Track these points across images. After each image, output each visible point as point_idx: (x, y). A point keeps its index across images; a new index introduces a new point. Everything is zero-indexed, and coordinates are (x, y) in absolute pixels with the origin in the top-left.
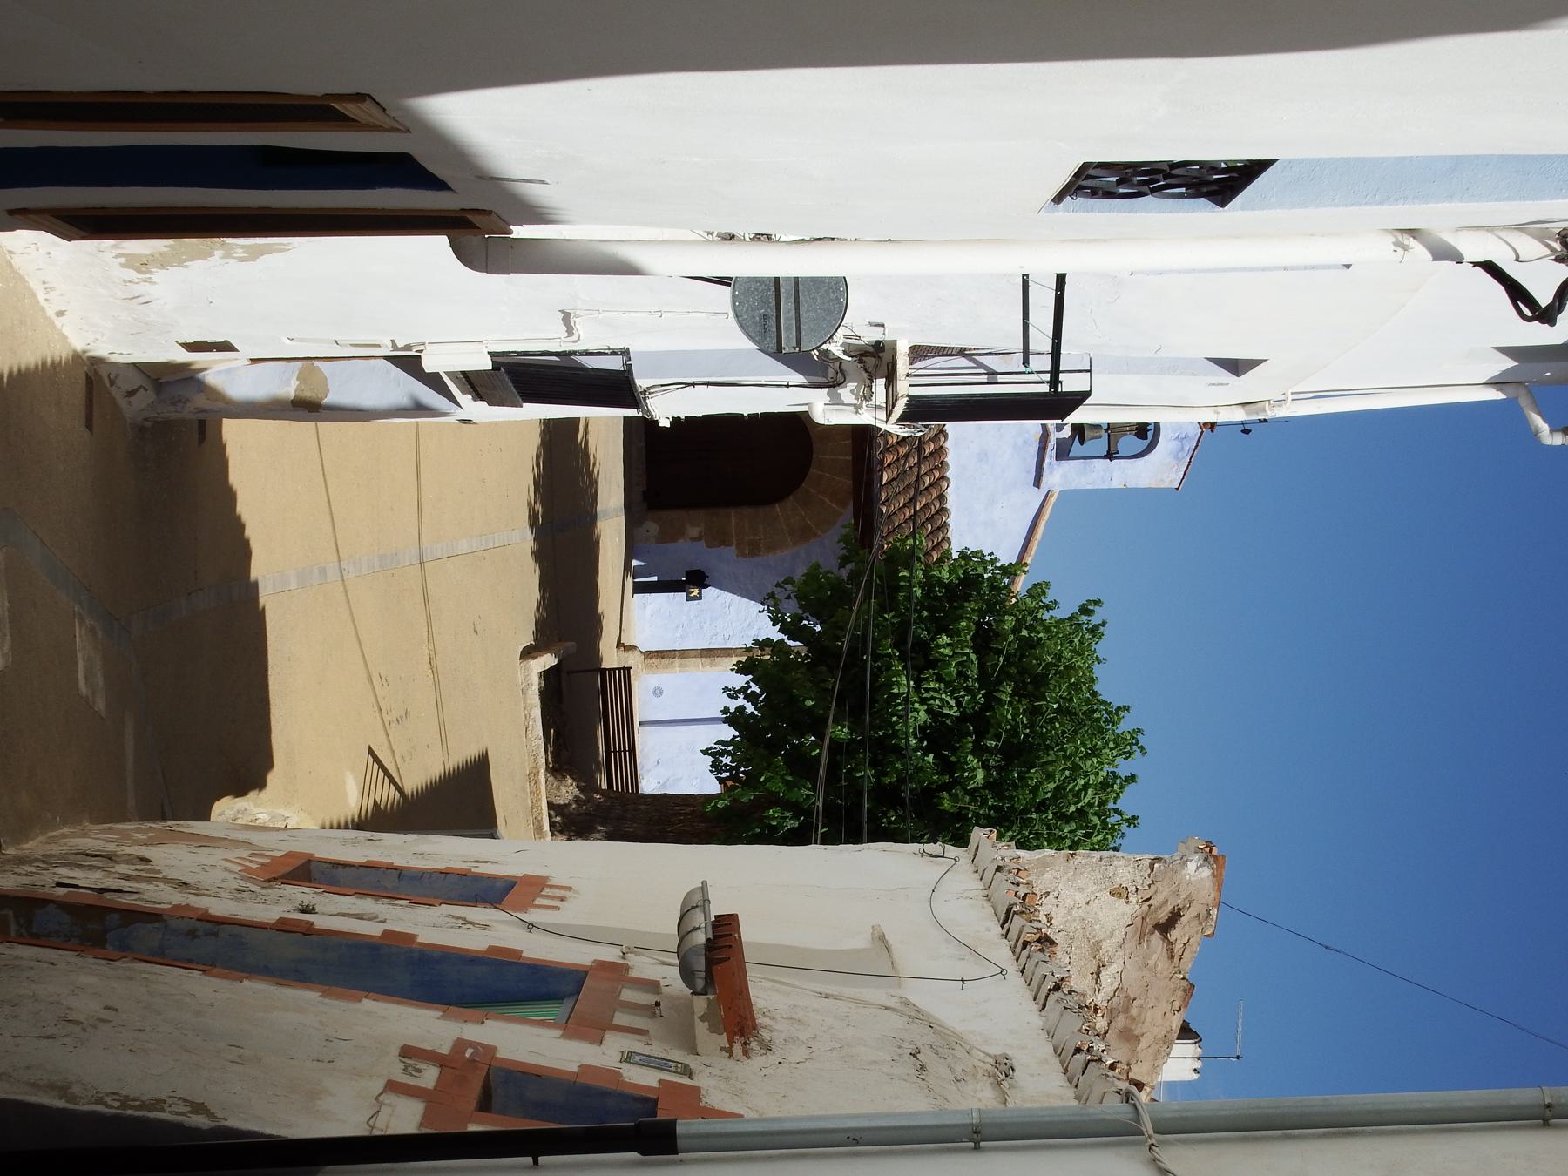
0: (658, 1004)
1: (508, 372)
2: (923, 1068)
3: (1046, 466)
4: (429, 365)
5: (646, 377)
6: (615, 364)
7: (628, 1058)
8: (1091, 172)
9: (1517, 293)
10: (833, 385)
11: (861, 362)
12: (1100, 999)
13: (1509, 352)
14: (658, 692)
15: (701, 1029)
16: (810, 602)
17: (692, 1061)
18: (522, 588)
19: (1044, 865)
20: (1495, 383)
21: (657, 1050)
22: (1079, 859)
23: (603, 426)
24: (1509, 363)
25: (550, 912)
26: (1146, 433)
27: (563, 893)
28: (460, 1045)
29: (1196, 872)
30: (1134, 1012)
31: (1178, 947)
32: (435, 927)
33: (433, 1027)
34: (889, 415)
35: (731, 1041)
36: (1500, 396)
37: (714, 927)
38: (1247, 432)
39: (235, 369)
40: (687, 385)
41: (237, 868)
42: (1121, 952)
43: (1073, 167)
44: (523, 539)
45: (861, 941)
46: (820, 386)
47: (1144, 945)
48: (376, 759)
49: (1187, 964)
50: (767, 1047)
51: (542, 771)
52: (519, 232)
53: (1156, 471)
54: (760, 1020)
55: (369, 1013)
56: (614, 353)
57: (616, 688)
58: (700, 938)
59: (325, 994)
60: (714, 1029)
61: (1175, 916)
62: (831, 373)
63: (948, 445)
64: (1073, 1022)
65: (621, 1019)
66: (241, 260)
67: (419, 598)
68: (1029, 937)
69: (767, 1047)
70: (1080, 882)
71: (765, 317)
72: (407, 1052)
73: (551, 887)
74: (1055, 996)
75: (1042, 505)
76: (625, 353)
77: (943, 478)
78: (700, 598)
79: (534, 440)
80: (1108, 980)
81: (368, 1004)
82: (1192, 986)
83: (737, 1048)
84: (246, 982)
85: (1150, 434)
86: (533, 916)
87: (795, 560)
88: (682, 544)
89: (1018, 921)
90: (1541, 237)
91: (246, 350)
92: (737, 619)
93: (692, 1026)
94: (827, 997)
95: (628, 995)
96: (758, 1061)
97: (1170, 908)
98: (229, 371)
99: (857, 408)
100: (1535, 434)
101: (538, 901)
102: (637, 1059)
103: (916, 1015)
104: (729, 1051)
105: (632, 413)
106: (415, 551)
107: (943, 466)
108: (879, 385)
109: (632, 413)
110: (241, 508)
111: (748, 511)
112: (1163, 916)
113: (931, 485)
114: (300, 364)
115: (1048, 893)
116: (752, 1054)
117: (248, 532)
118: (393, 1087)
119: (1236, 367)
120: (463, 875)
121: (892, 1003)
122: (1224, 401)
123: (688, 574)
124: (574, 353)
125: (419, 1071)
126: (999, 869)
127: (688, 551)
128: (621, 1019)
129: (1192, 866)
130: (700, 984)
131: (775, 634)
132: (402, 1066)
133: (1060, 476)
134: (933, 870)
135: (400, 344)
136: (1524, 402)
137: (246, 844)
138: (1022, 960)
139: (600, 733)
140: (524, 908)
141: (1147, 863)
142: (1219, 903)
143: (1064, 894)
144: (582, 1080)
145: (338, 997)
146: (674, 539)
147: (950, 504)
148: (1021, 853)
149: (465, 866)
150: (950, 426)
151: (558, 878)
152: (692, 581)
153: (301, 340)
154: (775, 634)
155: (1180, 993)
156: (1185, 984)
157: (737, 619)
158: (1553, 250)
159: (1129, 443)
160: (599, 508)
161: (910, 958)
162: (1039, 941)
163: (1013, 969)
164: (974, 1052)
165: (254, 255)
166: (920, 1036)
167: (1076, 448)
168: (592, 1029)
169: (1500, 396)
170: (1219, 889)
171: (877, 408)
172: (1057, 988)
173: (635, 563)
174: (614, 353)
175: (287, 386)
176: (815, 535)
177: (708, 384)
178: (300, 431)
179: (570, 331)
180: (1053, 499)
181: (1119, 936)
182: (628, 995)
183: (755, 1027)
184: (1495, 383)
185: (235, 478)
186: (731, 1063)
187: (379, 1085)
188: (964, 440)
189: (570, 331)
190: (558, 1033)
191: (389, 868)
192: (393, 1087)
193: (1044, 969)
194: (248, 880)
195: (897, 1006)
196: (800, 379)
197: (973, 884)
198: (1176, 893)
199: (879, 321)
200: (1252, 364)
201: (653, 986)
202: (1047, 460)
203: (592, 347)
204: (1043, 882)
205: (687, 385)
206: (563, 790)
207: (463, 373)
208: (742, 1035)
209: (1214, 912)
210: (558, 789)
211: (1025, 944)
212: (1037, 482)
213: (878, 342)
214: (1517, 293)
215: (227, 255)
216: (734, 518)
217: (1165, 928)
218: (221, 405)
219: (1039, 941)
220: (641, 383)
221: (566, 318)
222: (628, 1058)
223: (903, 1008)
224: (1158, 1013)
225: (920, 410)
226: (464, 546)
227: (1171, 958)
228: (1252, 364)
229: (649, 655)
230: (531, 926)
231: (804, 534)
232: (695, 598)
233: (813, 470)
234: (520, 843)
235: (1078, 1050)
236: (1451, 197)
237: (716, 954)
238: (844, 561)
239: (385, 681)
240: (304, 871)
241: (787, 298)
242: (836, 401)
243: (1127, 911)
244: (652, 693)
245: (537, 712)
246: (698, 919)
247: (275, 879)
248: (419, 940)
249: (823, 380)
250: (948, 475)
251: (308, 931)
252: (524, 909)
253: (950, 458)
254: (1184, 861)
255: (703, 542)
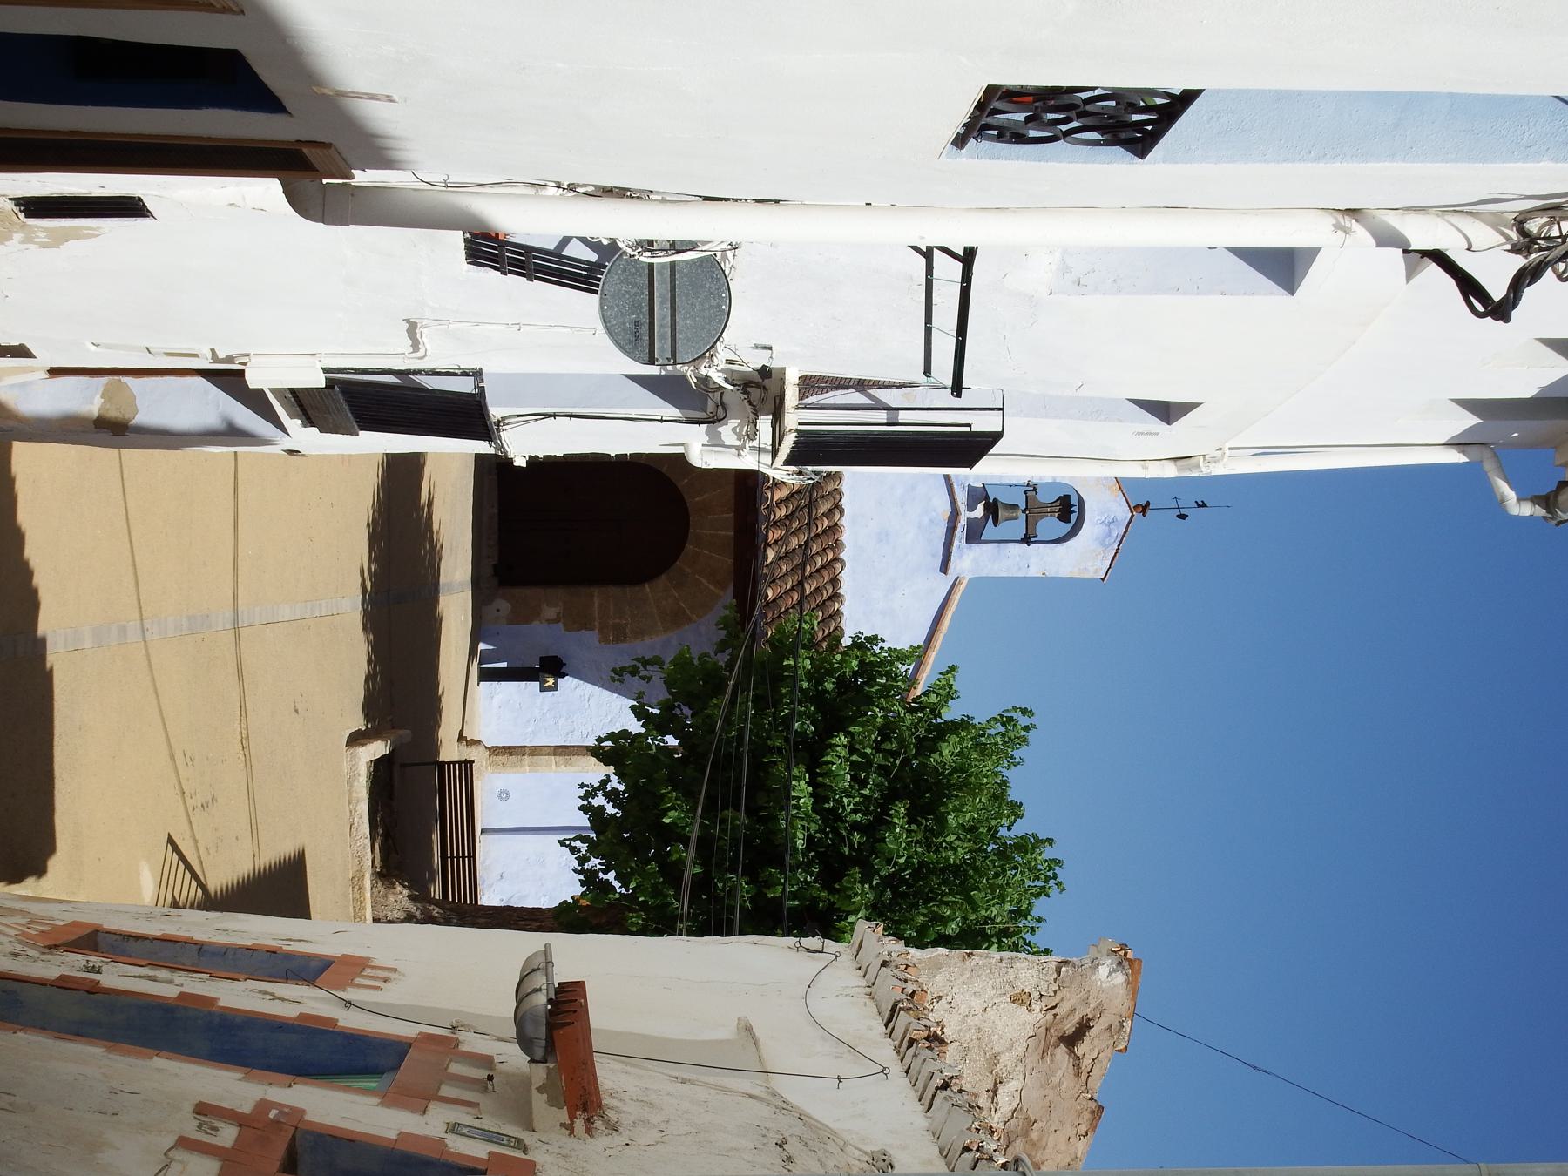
0: (490, 1078)
1: (343, 392)
2: (789, 1159)
3: (954, 549)
4: (253, 380)
5: (500, 405)
6: (466, 386)
7: (453, 1128)
8: (996, 104)
9: (1469, 286)
10: (713, 421)
11: (745, 392)
12: (996, 1120)
13: (1471, 405)
14: (504, 795)
15: (539, 1101)
16: (685, 694)
17: (527, 1137)
18: (348, 658)
19: (936, 965)
20: (1456, 444)
21: (488, 1123)
22: (975, 959)
23: (449, 460)
24: (1472, 420)
25: (372, 992)
26: (1068, 509)
27: (387, 975)
28: (264, 1106)
29: (1108, 978)
30: (1034, 1135)
31: (1086, 1063)
32: (238, 995)
33: (235, 1088)
34: (775, 454)
35: (572, 1117)
36: (1462, 459)
37: (557, 992)
38: (1183, 517)
39: (31, 383)
40: (547, 416)
41: (13, 932)
42: (1020, 1067)
43: (976, 94)
44: (349, 607)
45: (726, 1032)
46: (698, 422)
47: (1048, 1059)
48: (176, 849)
49: (1096, 1083)
50: (614, 1128)
51: (368, 875)
52: (361, 177)
53: (1081, 557)
54: (606, 1101)
55: (159, 1070)
56: (465, 374)
57: (456, 789)
58: (541, 1000)
59: (109, 1050)
60: (553, 1102)
61: (1083, 1028)
62: (711, 406)
63: (844, 522)
64: (963, 1120)
65: (446, 1091)
66: (44, 246)
67: (232, 668)
68: (915, 1035)
69: (614, 1128)
70: (977, 986)
71: (637, 323)
72: (202, 1109)
73: (373, 967)
74: (941, 1095)
75: (949, 594)
76: (477, 374)
77: (837, 559)
78: (555, 688)
79: (369, 483)
80: (1006, 1099)
81: (159, 1062)
82: (1101, 1108)
83: (579, 1124)
84: (20, 1034)
85: (1074, 517)
86: (351, 994)
87: (665, 644)
88: (537, 626)
89: (903, 1019)
90: (1495, 222)
91: (47, 357)
92: (595, 709)
93: (529, 1102)
94: (684, 1081)
95: (456, 1068)
96: (602, 1141)
97: (1077, 1017)
98: (23, 385)
99: (739, 449)
100: (1502, 501)
101: (358, 981)
102: (465, 1131)
103: (785, 1107)
104: (570, 1128)
105: (483, 447)
106: (229, 614)
107: (837, 545)
108: (765, 423)
109: (483, 447)
110: (29, 552)
111: (614, 591)
112: (1069, 1027)
113: (823, 567)
114: (105, 380)
115: (940, 998)
116: (596, 1134)
117: (37, 580)
118: (184, 1143)
119: (1167, 412)
120: (273, 952)
121: (756, 1092)
122: (1150, 453)
123: (543, 660)
124: (417, 372)
125: (216, 1129)
126: (884, 964)
127: (544, 635)
128: (446, 1091)
129: (1103, 971)
130: (539, 1053)
131: (636, 727)
132: (196, 1123)
133: (970, 560)
134: (812, 965)
135: (222, 355)
136: (1489, 466)
137: (23, 913)
138: (907, 1060)
139: (436, 837)
140: (342, 986)
141: (1053, 966)
142: (1133, 1015)
143: (958, 999)
144: (401, 1147)
145: (128, 1053)
146: (527, 620)
147: (844, 590)
148: (912, 951)
149: (275, 944)
150: (848, 471)
151: (381, 957)
152: (548, 669)
153: (108, 347)
154: (636, 727)
155: (1087, 1116)
156: (1093, 1105)
157: (595, 709)
158: (1508, 239)
159: (1050, 525)
160: (442, 580)
161: (778, 1054)
162: (927, 1039)
163: (896, 1069)
164: (849, 1149)
165: (58, 240)
166: (787, 1126)
167: (990, 530)
168: (419, 1098)
169: (1462, 459)
170: (1134, 998)
171: (760, 450)
172: (945, 1086)
173: (482, 646)
174: (465, 374)
175: (86, 399)
176: (689, 620)
177: (571, 416)
178: (103, 458)
179: (416, 346)
180: (962, 587)
181: (1020, 1049)
182: (456, 1068)
183: (600, 1106)
184: (1456, 444)
185: (24, 517)
186: (572, 1142)
187: (170, 1140)
188: (859, 484)
189: (416, 346)
190: (375, 1100)
191: (189, 942)
192: (184, 1143)
193: (931, 1067)
194: (27, 944)
195: (764, 1095)
196: (675, 413)
197: (855, 981)
198: (1086, 1001)
199: (767, 343)
200: (1185, 408)
201: (487, 1061)
202: (956, 543)
203: (440, 366)
204: (936, 983)
205: (547, 416)
206: (391, 898)
207: (292, 391)
208: (585, 1110)
209: (1127, 1024)
210: (385, 896)
211: (912, 1042)
212: (944, 567)
213: (764, 367)
214: (1469, 286)
215: (28, 240)
216: (597, 598)
217: (1071, 1041)
218: (11, 423)
219: (927, 1039)
220: (495, 412)
221: (412, 328)
222: (453, 1128)
223: (769, 1097)
224: (1061, 1138)
225: (811, 449)
226: (286, 613)
227: (1078, 1074)
228: (1185, 408)
229: (495, 751)
230: (349, 1004)
231: (677, 619)
232: (550, 689)
233: (689, 547)
234: (344, 913)
235: (966, 1149)
236: (1392, 157)
237: (557, 1023)
238: (722, 647)
239: (190, 761)
240: (91, 940)
241: (662, 303)
242: (715, 442)
243: (1026, 1021)
244: (498, 797)
245: (364, 808)
246: (539, 980)
247: (56, 946)
248: (220, 1004)
249: (703, 415)
250: (843, 556)
251: (94, 989)
252: (342, 987)
253: (845, 538)
254: (1095, 966)
255: (561, 625)
